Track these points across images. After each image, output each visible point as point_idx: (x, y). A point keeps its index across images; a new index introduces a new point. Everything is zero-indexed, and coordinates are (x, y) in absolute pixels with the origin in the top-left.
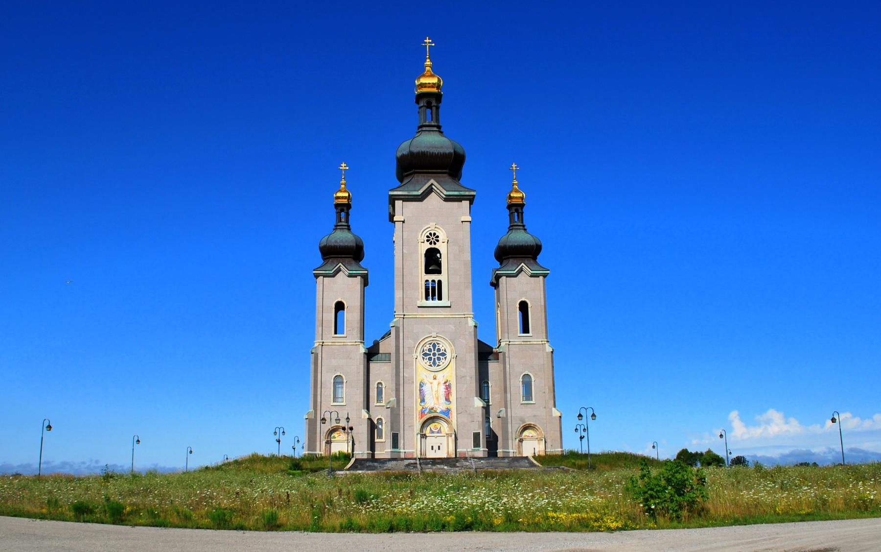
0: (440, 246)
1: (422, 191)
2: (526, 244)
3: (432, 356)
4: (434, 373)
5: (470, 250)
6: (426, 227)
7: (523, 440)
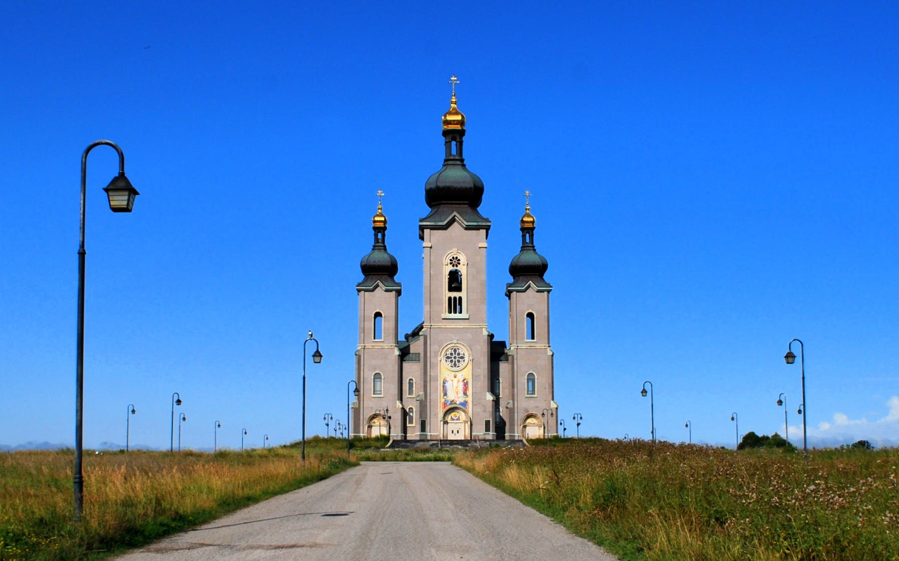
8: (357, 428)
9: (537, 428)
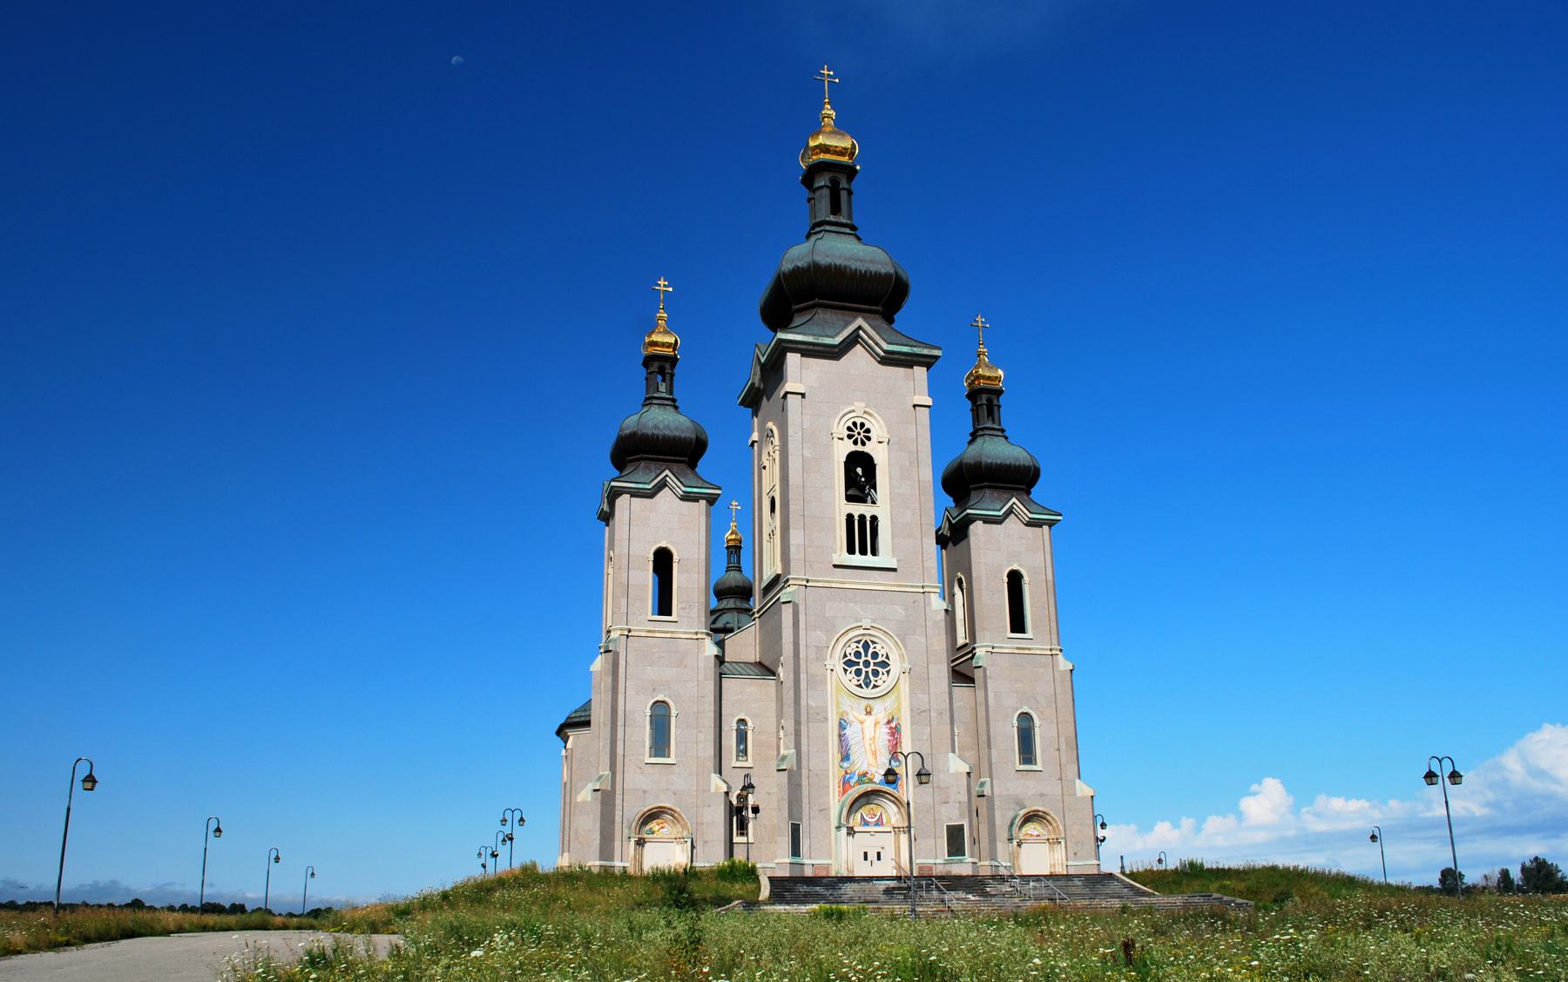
0: (873, 450)
1: (841, 339)
2: (1017, 464)
3: (861, 666)
4: (866, 701)
5: (930, 461)
6: (845, 411)
7: (645, 842)
8: (606, 850)
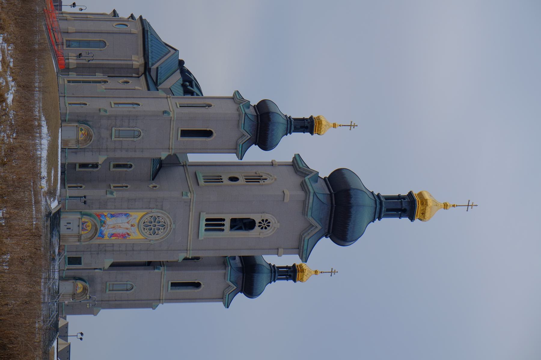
9: (69, 32)
